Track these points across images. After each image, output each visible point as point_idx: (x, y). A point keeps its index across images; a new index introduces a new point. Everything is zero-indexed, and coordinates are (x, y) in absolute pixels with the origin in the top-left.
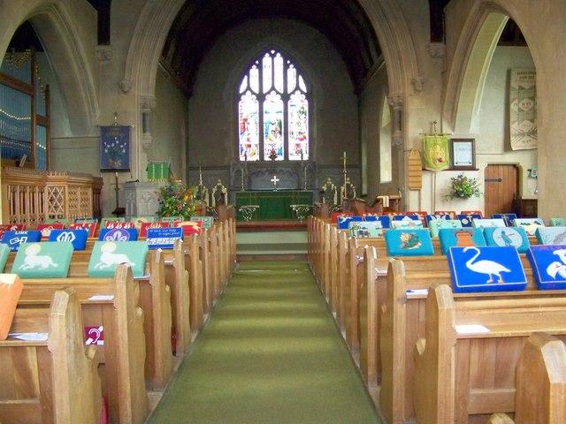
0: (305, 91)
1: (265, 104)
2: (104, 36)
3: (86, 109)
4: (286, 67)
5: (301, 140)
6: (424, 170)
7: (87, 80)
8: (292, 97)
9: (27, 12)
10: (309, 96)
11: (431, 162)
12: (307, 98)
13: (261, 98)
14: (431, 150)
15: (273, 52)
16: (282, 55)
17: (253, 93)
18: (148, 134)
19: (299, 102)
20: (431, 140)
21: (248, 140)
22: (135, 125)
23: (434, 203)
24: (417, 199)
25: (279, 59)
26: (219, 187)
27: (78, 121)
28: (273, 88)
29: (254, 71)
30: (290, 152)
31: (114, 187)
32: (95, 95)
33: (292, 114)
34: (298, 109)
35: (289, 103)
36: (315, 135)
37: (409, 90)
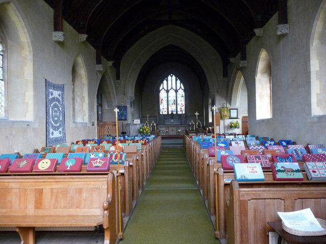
4: (176, 80)
10: (185, 91)
13: (168, 91)
19: (181, 93)
25: (174, 77)
28: (172, 88)
29: (165, 82)
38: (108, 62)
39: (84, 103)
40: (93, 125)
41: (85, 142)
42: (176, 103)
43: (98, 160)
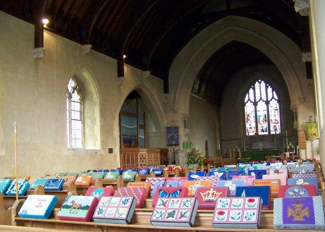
0: (277, 98)
1: (258, 106)
2: (166, 90)
3: (160, 120)
4: (267, 87)
5: (276, 123)
6: (307, 139)
7: (159, 108)
8: (271, 102)
9: (132, 88)
10: (279, 101)
11: (310, 135)
12: (278, 102)
13: (255, 104)
14: (310, 130)
15: (260, 81)
16: (264, 82)
17: (251, 102)
18: (187, 129)
19: (274, 104)
20: (309, 125)
21: (250, 125)
22: (180, 124)
23: (313, 154)
24: (307, 154)
25: (263, 84)
26: (236, 149)
27: (158, 125)
28: (261, 99)
29: (251, 91)
30: (259, 130)
31: (173, 152)
32: (164, 116)
33: (271, 111)
34: (274, 108)
35: (269, 106)
36: (282, 120)
37: (298, 102)
38: (144, 73)
39: (95, 126)
40: (111, 151)
41: (89, 171)
42: (267, 119)
43: (211, 191)
